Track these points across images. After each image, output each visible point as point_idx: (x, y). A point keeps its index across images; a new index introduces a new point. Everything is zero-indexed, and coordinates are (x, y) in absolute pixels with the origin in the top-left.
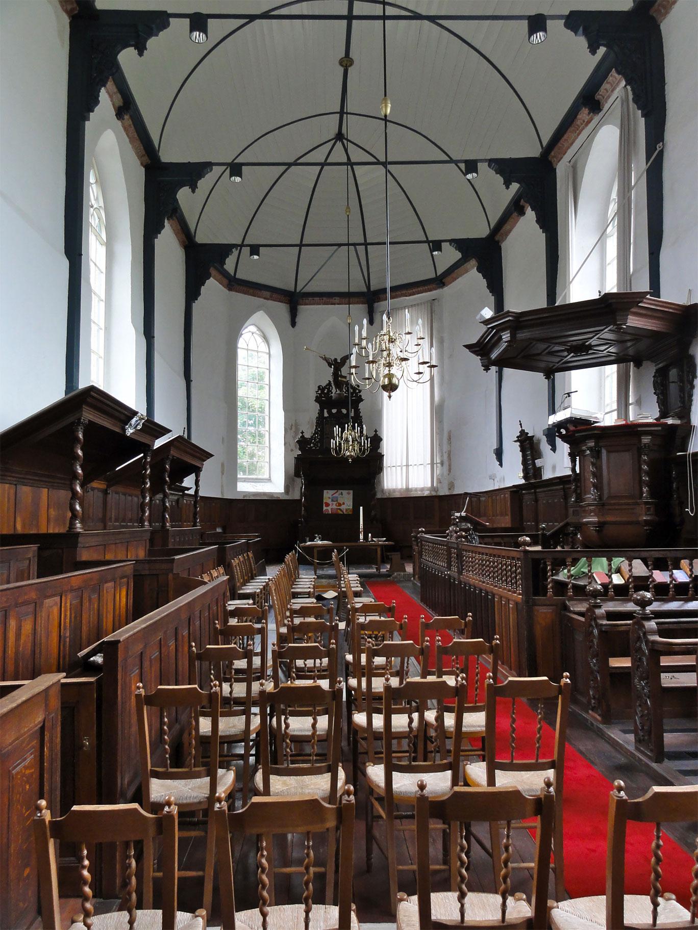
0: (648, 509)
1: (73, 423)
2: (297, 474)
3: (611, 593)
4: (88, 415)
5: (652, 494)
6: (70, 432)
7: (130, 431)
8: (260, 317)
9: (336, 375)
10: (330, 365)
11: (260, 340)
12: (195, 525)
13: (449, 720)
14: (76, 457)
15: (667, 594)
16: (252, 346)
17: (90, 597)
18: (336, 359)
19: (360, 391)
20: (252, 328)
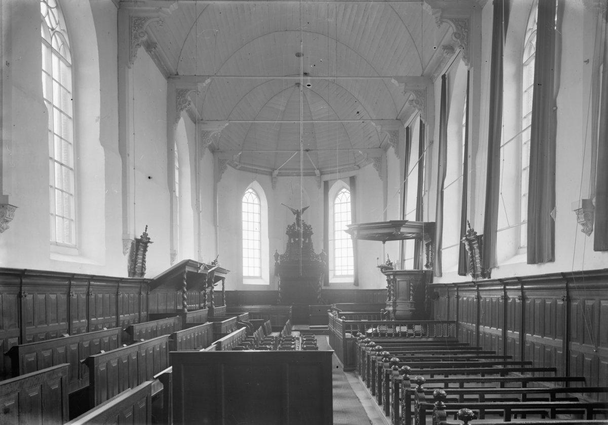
0: (411, 306)
1: (182, 273)
2: (276, 274)
3: (380, 335)
4: (188, 269)
5: (414, 299)
6: (182, 274)
7: (199, 271)
8: (255, 184)
9: (298, 220)
10: (294, 213)
11: (254, 197)
12: (224, 305)
13: (126, 295)
14: (184, 285)
15: (371, 336)
16: (251, 201)
17: (412, 388)
18: (298, 210)
19: (311, 229)
20: (250, 190)
